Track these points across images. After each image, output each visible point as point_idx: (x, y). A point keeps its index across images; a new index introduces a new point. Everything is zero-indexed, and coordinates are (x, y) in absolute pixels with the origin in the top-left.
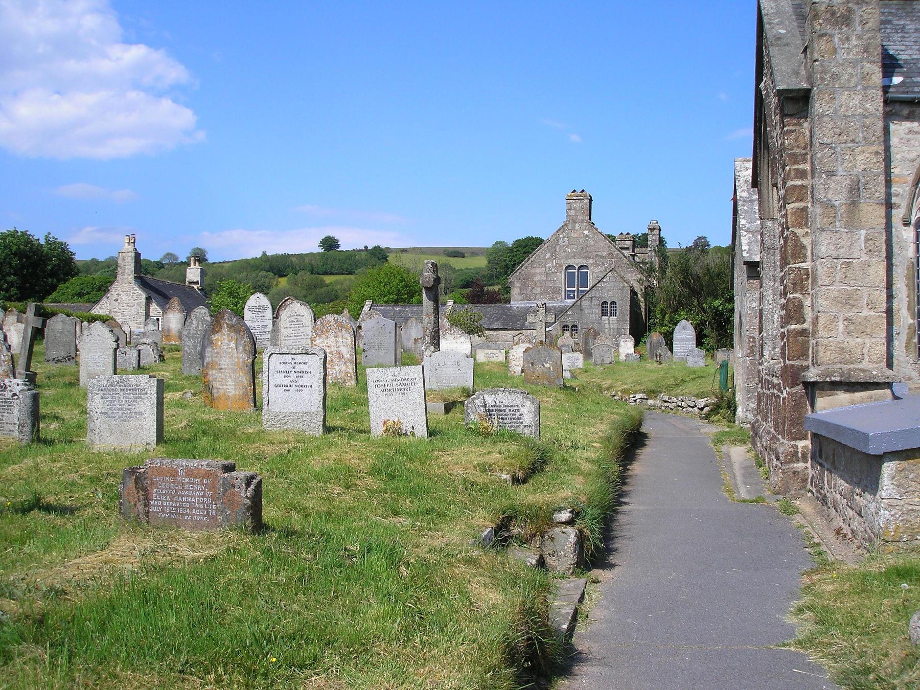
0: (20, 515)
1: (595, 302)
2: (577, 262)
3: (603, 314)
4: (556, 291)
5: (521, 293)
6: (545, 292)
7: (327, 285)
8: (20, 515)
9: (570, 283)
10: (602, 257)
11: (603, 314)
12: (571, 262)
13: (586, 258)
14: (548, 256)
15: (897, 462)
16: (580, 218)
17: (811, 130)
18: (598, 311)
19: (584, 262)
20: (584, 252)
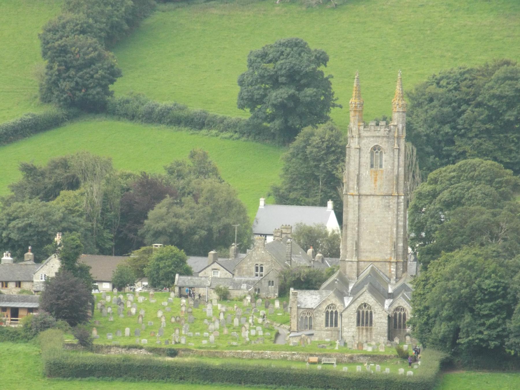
0: (304, 8)
1: (266, 281)
2: (259, 263)
3: (269, 285)
4: (252, 273)
5: (238, 274)
6: (247, 274)
7: (99, 349)
8: (304, 8)
9: (257, 271)
10: (269, 262)
11: (269, 285)
12: (257, 263)
13: (263, 261)
14: (248, 260)
15: (341, 370)
16: (261, 246)
17: (472, 155)
18: (267, 284)
19: (262, 263)
20: (262, 260)
